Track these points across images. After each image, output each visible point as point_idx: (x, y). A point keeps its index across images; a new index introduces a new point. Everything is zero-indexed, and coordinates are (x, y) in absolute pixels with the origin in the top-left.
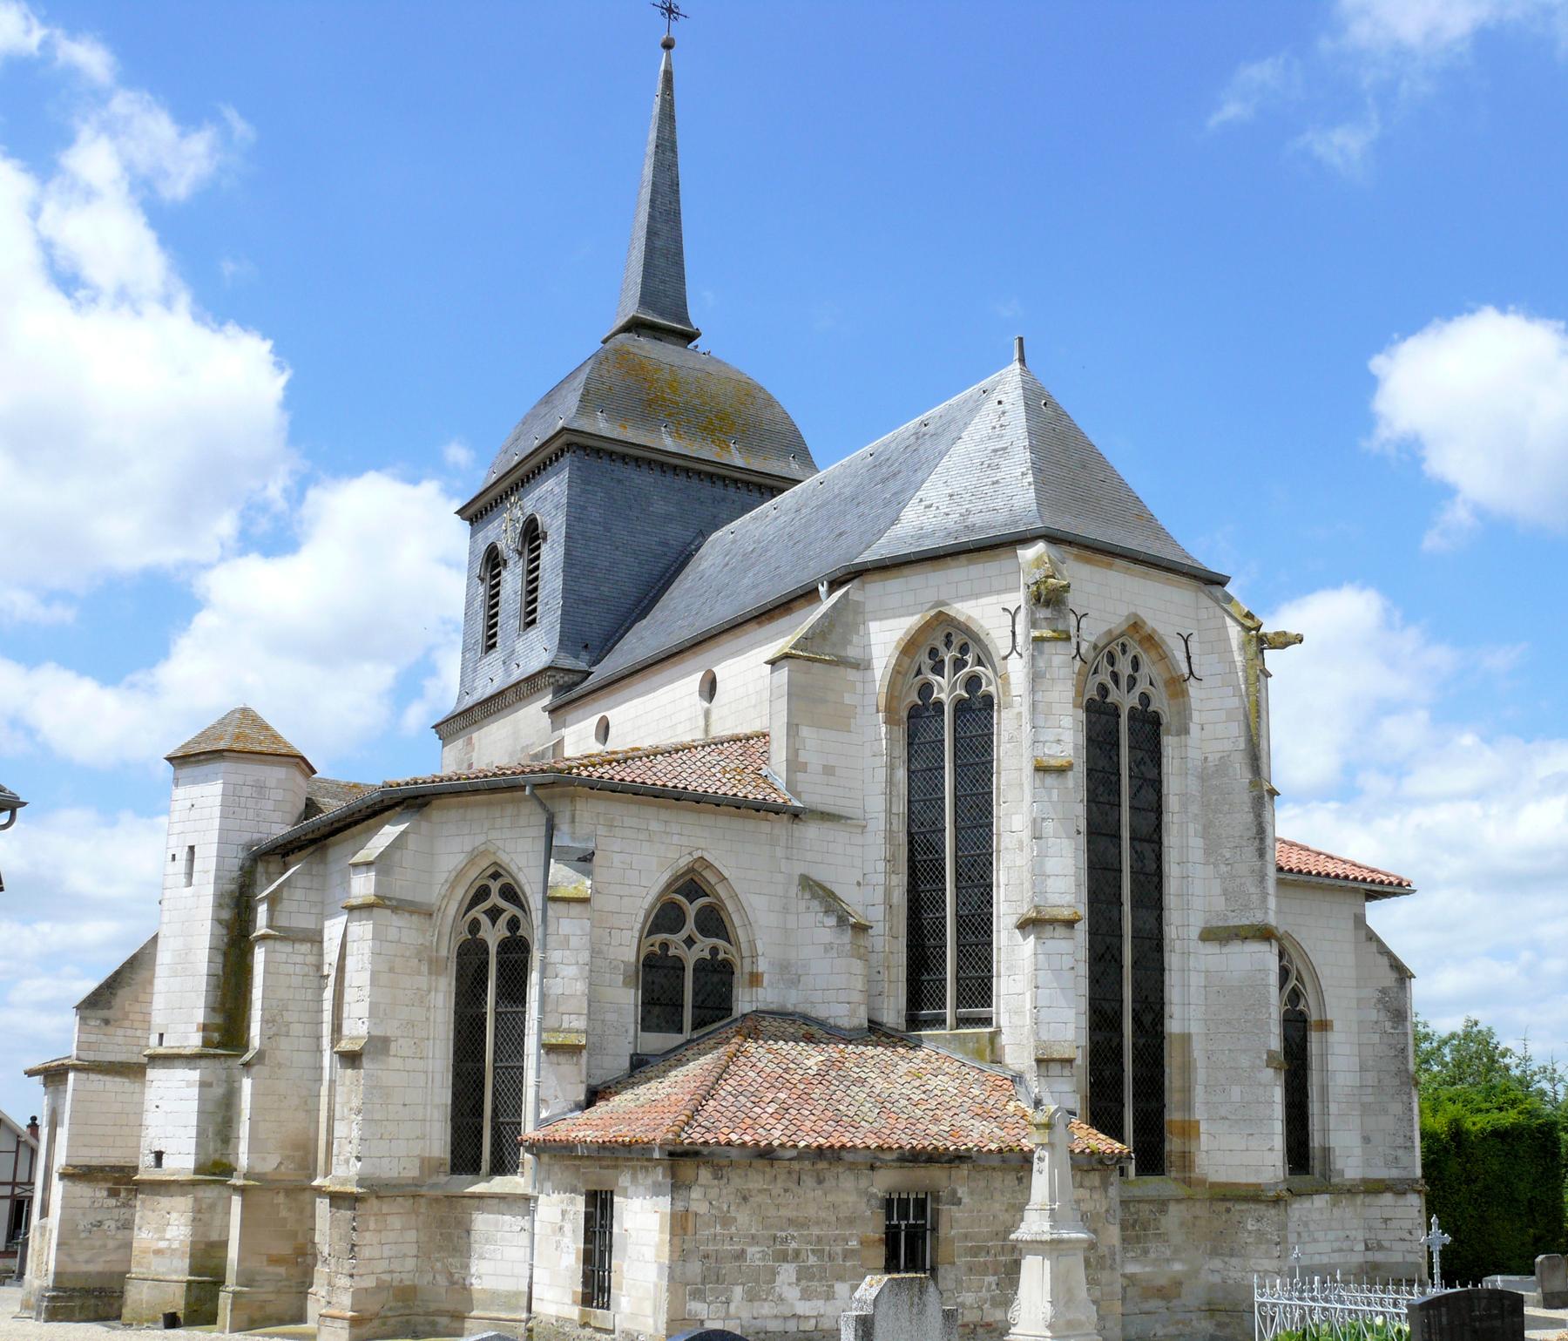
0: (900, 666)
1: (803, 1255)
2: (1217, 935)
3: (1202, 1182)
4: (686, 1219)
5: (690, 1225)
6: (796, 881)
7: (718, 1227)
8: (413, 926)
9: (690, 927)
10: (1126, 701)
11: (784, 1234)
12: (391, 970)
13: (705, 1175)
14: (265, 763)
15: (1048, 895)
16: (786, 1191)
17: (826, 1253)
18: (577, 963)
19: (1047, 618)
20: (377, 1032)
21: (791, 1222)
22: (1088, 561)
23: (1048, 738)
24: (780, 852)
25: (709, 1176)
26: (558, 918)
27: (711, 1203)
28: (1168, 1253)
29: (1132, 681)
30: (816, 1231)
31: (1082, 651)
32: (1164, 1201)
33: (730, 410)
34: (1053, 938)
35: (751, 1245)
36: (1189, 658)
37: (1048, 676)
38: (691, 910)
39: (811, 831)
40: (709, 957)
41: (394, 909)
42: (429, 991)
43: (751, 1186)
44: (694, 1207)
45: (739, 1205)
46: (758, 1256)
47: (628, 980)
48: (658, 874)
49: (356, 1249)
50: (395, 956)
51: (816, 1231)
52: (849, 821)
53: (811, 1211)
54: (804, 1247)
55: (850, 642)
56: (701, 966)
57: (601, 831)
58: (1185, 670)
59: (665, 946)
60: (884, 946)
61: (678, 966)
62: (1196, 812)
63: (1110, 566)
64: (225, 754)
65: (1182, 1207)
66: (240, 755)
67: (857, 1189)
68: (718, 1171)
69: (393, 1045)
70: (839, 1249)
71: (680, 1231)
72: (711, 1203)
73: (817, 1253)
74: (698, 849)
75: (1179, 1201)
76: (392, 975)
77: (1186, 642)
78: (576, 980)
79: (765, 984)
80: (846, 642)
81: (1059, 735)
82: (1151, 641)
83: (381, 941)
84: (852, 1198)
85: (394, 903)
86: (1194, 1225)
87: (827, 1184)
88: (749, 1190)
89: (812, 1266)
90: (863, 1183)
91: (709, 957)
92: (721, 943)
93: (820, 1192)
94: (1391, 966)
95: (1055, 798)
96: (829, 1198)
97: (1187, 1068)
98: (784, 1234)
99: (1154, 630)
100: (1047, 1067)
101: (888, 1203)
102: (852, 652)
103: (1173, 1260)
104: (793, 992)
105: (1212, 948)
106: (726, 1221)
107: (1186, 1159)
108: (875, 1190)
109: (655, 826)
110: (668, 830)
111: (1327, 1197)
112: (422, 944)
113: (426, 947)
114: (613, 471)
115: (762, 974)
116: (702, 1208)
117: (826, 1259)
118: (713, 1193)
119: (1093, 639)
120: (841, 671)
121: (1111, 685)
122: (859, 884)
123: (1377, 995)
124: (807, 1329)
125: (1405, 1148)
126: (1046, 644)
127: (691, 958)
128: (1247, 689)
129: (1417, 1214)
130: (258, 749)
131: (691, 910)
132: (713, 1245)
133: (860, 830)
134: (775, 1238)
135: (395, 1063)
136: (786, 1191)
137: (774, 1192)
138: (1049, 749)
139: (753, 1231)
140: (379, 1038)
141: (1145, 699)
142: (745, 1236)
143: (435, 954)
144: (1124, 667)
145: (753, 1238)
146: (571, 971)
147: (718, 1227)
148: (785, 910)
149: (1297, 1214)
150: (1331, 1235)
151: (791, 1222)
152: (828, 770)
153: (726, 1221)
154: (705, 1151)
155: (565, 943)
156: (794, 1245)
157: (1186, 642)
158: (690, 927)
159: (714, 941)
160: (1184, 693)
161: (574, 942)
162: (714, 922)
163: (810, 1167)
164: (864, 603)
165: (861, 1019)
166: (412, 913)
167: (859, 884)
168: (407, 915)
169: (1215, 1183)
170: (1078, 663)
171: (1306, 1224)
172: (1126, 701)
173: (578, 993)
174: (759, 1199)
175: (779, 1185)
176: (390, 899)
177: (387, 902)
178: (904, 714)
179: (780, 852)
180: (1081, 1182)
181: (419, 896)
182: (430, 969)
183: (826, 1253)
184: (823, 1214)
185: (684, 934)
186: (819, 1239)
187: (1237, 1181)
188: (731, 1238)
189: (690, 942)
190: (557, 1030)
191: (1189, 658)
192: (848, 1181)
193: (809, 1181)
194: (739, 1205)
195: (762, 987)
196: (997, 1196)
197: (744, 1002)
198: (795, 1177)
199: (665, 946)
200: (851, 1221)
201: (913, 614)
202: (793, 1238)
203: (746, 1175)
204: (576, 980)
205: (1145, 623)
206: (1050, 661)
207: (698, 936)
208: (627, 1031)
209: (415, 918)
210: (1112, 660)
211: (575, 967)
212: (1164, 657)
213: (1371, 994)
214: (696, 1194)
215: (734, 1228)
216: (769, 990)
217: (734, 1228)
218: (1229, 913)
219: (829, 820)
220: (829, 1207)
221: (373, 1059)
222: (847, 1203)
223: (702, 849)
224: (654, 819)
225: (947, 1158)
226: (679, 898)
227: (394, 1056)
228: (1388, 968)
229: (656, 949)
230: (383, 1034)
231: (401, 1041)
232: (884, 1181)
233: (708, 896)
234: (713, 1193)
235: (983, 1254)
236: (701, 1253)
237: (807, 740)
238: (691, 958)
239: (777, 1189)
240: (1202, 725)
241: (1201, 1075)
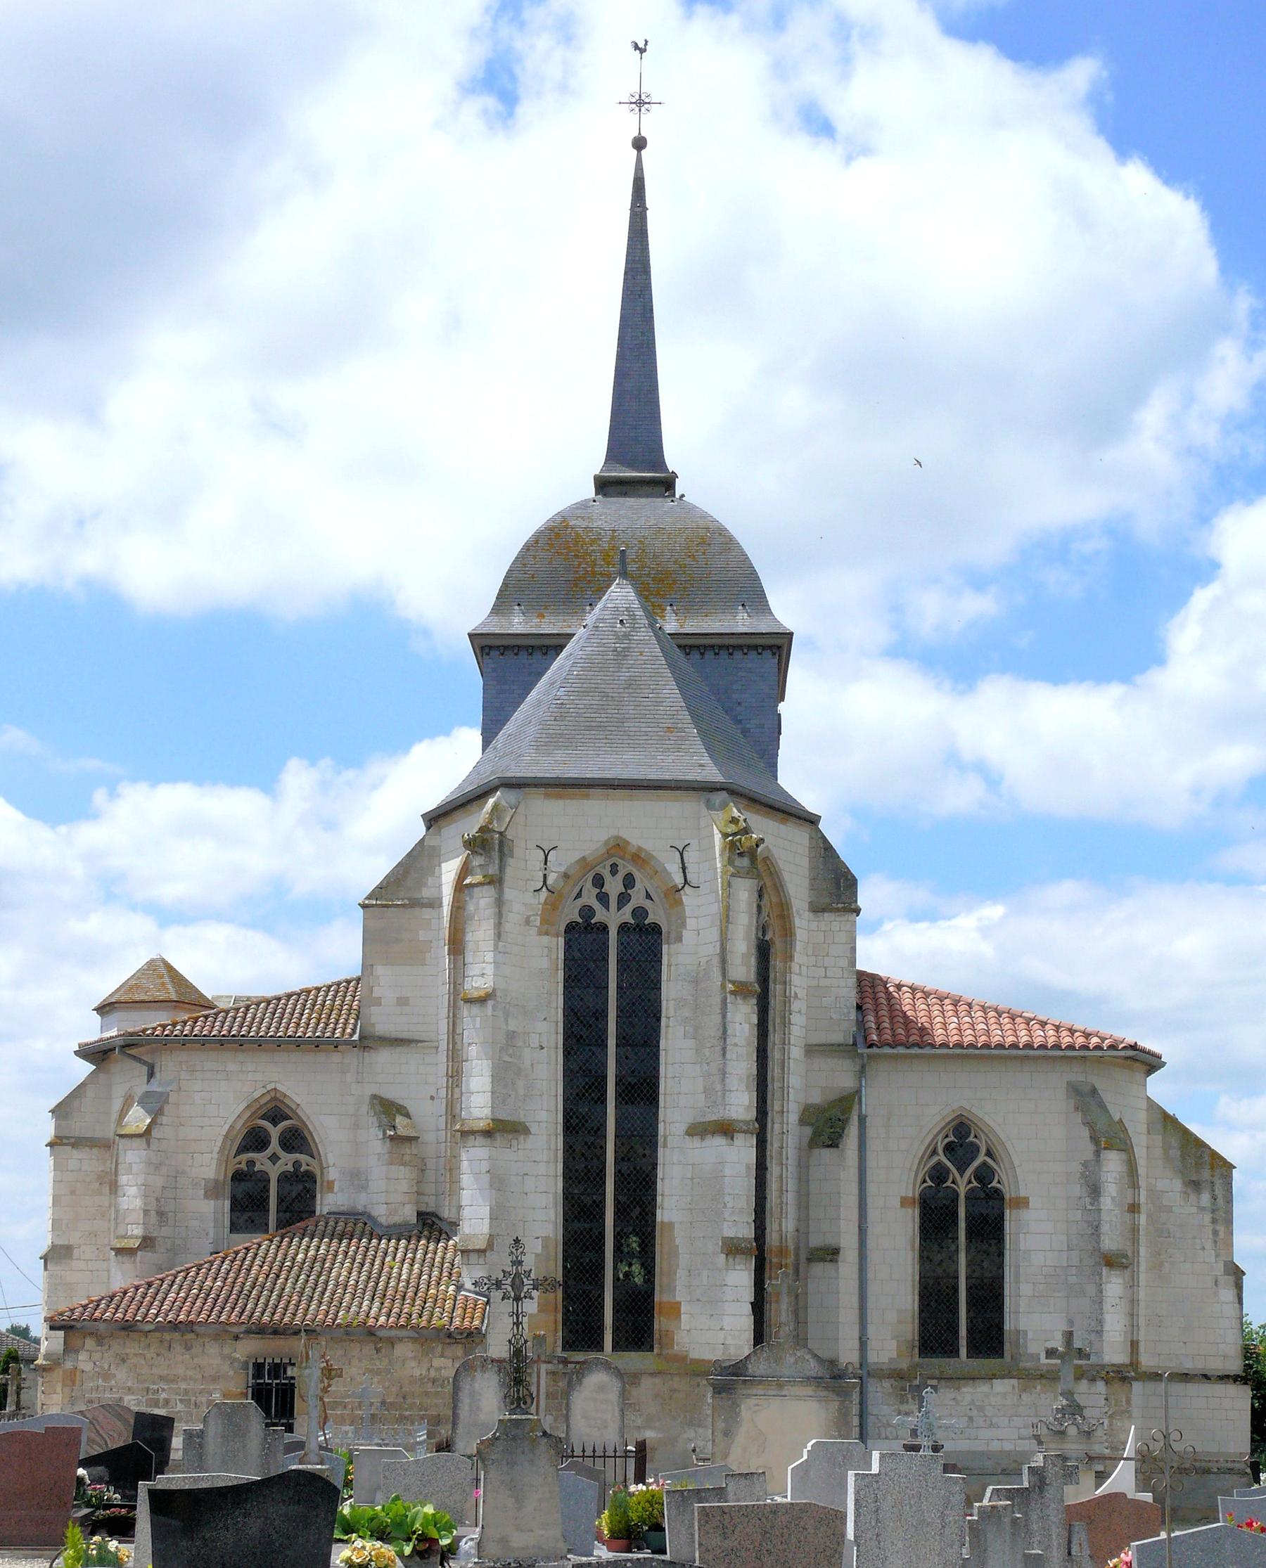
0: (458, 902)
1: (172, 1403)
2: (699, 1130)
3: (682, 1359)
4: (75, 1375)
5: (78, 1378)
6: (367, 1100)
7: (100, 1381)
8: (93, 1157)
9: (274, 1146)
10: (613, 918)
11: (156, 1387)
12: (73, 1193)
13: (90, 1343)
14: (148, 1009)
15: (472, 1110)
16: (158, 1355)
17: (192, 1402)
18: (137, 1185)
19: (480, 865)
20: (59, 1242)
21: (161, 1378)
22: (560, 797)
23: (475, 973)
24: (350, 1077)
25: (93, 1343)
26: (125, 1150)
27: (95, 1364)
28: (639, 1422)
29: (623, 899)
30: (183, 1386)
31: (549, 882)
32: (635, 1374)
33: (674, 567)
34: (473, 1147)
35: (127, 1394)
36: (684, 869)
37: (476, 918)
38: (275, 1132)
39: (383, 1058)
40: (292, 1170)
41: (74, 1146)
42: (110, 1207)
43: (128, 1351)
44: (81, 1366)
45: (118, 1365)
46: (133, 1402)
47: (209, 1193)
48: (235, 1106)
49: (44, 1407)
50: (77, 1181)
51: (183, 1386)
52: (419, 1044)
53: (180, 1371)
54: (173, 1397)
55: (425, 884)
56: (284, 1178)
57: (183, 1075)
58: (678, 879)
59: (251, 1163)
60: (446, 1151)
61: (264, 1178)
62: (687, 1015)
63: (587, 797)
64: (116, 1005)
65: (657, 1380)
66: (127, 1005)
67: (221, 1355)
68: (100, 1339)
69: (76, 1252)
70: (204, 1399)
71: (69, 1383)
72: (95, 1364)
73: (186, 1402)
74: (271, 1082)
75: (652, 1374)
76: (74, 1197)
77: (681, 855)
78: (136, 1197)
79: (335, 1190)
80: (421, 883)
81: (484, 968)
82: (640, 858)
83: (62, 1171)
84: (216, 1361)
85: (73, 1140)
86: (671, 1398)
87: (194, 1350)
88: (127, 1354)
89: (180, 1412)
90: (227, 1350)
91: (292, 1170)
92: (303, 1158)
93: (188, 1356)
94: (1091, 1137)
95: (478, 1026)
96: (196, 1361)
97: (674, 1252)
98: (156, 1387)
99: (640, 849)
100: (468, 1256)
101: (258, 1368)
102: (426, 893)
103: (644, 1428)
104: (363, 1195)
105: (696, 1142)
106: (107, 1376)
107: (668, 1336)
108: (238, 1356)
109: (232, 1067)
110: (244, 1069)
111: (1014, 1381)
112: (102, 1171)
113: (107, 1173)
114: (530, 665)
115: (333, 1182)
116: (88, 1367)
117: (192, 1406)
118: (97, 1356)
119: (562, 869)
120: (417, 911)
121: (597, 906)
122: (432, 1098)
123: (1080, 1168)
124: (176, 1458)
125: (1097, 1331)
126: (476, 890)
127: (274, 1172)
128: (722, 893)
129: (1104, 1402)
130: (146, 998)
131: (275, 1132)
132: (96, 1393)
133: (434, 1051)
134: (148, 1390)
135: (76, 1264)
136: (158, 1355)
137: (148, 1356)
138: (476, 982)
139: (129, 1384)
140: (62, 1246)
141: (640, 912)
142: (123, 1388)
143: (114, 1177)
144: (614, 887)
145: (129, 1389)
146: (132, 1191)
147: (100, 1381)
148: (356, 1126)
149: (968, 1398)
150: (1018, 1422)
151: (162, 1378)
152: (402, 1001)
153: (107, 1376)
154: (78, 1325)
155: (129, 1171)
156: (164, 1395)
157: (681, 855)
158: (274, 1146)
159: (297, 1156)
160: (680, 902)
161: (135, 1168)
162: (296, 1140)
163: (179, 1337)
164: (440, 847)
165: (408, 1214)
166: (91, 1147)
167: (432, 1098)
168: (87, 1149)
169: (695, 1360)
170: (544, 893)
171: (981, 1409)
172: (613, 918)
173: (138, 1207)
174: (135, 1360)
175: (152, 1351)
176: (68, 1138)
177: (65, 1141)
178: (562, 928)
179: (350, 1077)
180: (442, 1353)
181: (98, 1134)
182: (110, 1190)
183: (192, 1402)
184: (190, 1373)
185: (269, 1152)
186: (186, 1392)
187: (702, 1357)
188: (111, 1389)
189: (274, 1158)
190: (124, 1237)
191: (684, 869)
192: (213, 1349)
193: (178, 1348)
194: (118, 1365)
195: (332, 1192)
196: (355, 1362)
197: (326, 1203)
198: (166, 1344)
199: (251, 1163)
200: (215, 1379)
201: (459, 856)
202: (163, 1390)
203: (125, 1343)
204: (136, 1197)
205: (628, 843)
206: (478, 903)
207: (281, 1153)
208: (207, 1234)
209: (95, 1150)
210: (598, 881)
211: (135, 1188)
212: (658, 872)
213: (1076, 1167)
214: (83, 1356)
215: (113, 1382)
216: (339, 1195)
217: (113, 1382)
218: (706, 1109)
219: (398, 1045)
220: (195, 1368)
221: (56, 1263)
222: (212, 1364)
223: (276, 1082)
224: (231, 1062)
225: (292, 1331)
226: (266, 1124)
227: (77, 1259)
228: (1089, 1139)
229: (244, 1167)
230: (66, 1243)
231: (83, 1248)
232: (248, 1348)
233: (291, 1119)
234: (97, 1356)
235: (340, 1408)
236: (86, 1400)
237: (381, 978)
238: (274, 1172)
239: (150, 1354)
240: (698, 931)
241: (684, 1260)
